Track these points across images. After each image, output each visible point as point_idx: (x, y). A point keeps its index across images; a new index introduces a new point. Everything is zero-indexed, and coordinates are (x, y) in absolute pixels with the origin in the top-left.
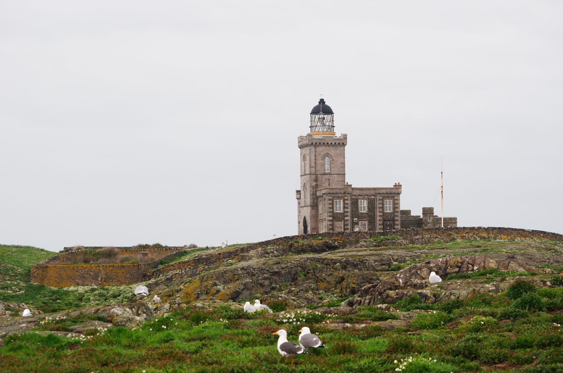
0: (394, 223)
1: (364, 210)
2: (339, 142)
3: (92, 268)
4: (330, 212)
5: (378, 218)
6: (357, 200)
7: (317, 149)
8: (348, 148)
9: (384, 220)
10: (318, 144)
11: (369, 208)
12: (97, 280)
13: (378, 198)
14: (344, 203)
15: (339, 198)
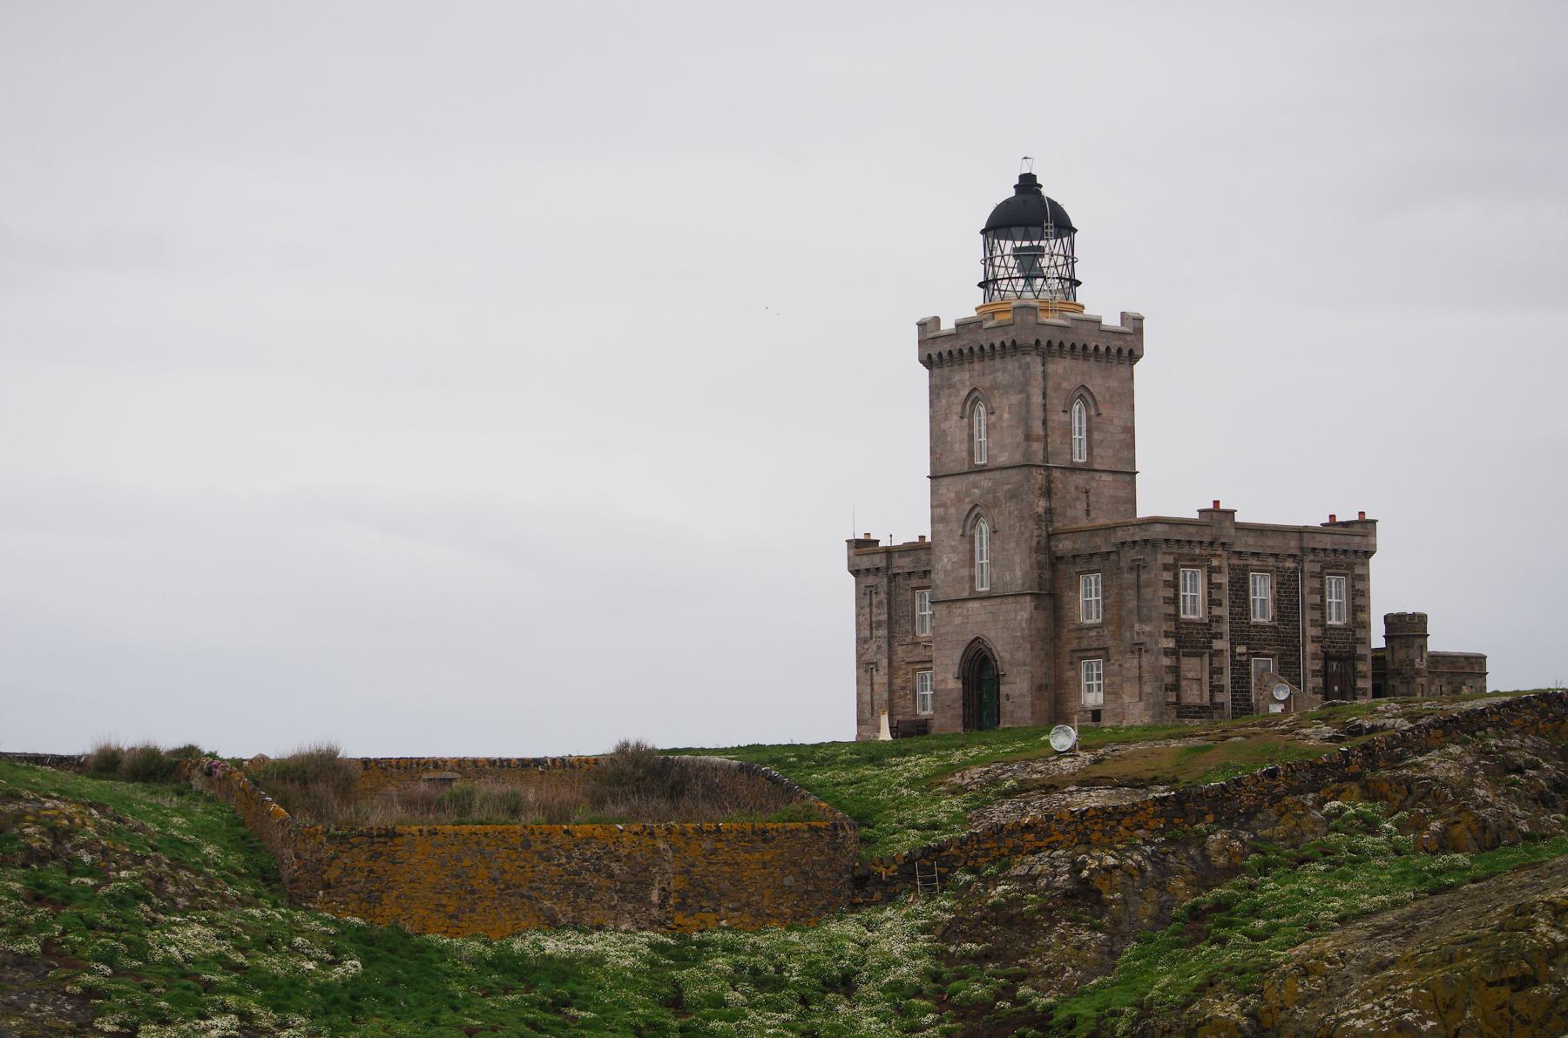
0: (1355, 668)
1: (1194, 611)
2: (1120, 343)
3: (617, 842)
4: (1168, 617)
5: (1311, 648)
6: (1244, 571)
7: (1051, 368)
8: (1148, 378)
9: (1327, 658)
10: (1055, 346)
11: (1278, 602)
12: (643, 900)
13: (1308, 567)
14: (1210, 582)
15: (1194, 562)
